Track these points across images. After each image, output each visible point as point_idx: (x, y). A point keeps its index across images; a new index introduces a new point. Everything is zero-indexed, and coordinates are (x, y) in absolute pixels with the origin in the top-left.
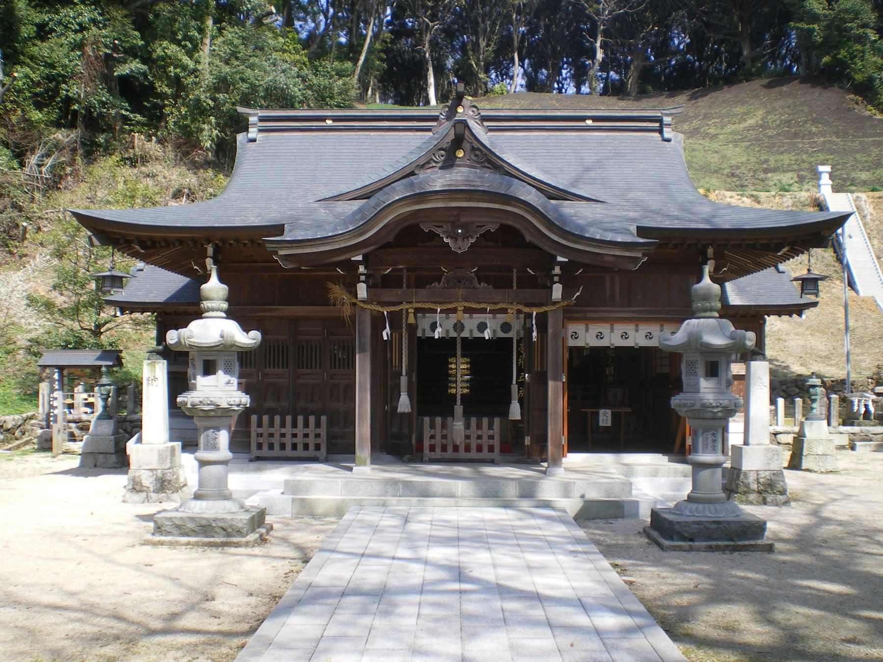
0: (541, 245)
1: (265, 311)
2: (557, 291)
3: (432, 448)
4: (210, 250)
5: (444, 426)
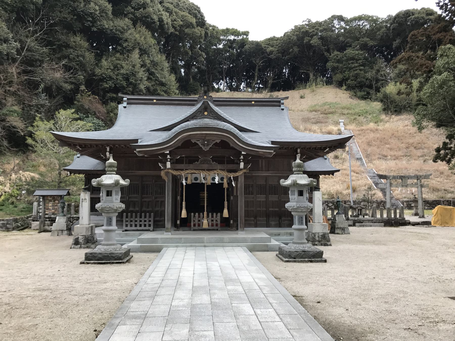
0: (236, 148)
1: (130, 173)
2: (242, 165)
4: (108, 149)
5: (199, 217)
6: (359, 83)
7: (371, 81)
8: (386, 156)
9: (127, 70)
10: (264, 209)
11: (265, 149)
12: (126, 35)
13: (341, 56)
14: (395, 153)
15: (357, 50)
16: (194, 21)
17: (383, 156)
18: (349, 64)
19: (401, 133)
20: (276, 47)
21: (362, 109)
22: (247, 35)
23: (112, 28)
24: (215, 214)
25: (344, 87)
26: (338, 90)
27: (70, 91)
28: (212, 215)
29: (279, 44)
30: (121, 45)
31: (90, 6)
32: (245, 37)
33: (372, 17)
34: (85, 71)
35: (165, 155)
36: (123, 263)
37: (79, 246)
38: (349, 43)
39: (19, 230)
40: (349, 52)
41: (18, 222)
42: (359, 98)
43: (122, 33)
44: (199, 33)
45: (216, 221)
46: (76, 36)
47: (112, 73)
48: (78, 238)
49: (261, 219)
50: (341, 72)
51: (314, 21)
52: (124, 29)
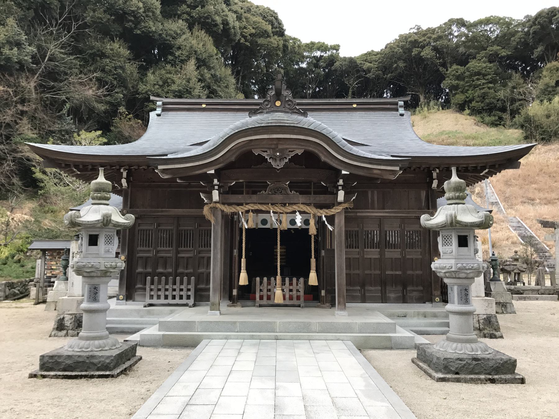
1: (158, 212)
2: (341, 196)
3: (261, 298)
5: (269, 283)
6: (488, 106)
7: (505, 102)
8: (533, 200)
9: (178, 86)
10: (378, 272)
11: (384, 165)
12: (180, 41)
13: (462, 71)
14: (546, 195)
15: (485, 62)
16: (269, 28)
17: (529, 200)
18: (473, 81)
19: (553, 168)
20: (375, 63)
21: (493, 138)
22: (337, 50)
23: (161, 32)
24: (295, 280)
25: (467, 111)
26: (458, 115)
27: (105, 113)
28: (291, 280)
29: (379, 59)
30: (172, 54)
31: (132, 3)
32: (334, 51)
33: (504, 19)
34: (126, 88)
35: (208, 179)
36: (113, 376)
37: (64, 332)
38: (471, 55)
39: (15, 300)
40: (472, 64)
41: (15, 288)
42: (487, 124)
43: (174, 38)
44: (276, 43)
45: (298, 291)
46: (114, 42)
47: (160, 90)
48: (64, 318)
49: (373, 288)
50: (462, 92)
51: (424, 28)
52: (177, 34)
